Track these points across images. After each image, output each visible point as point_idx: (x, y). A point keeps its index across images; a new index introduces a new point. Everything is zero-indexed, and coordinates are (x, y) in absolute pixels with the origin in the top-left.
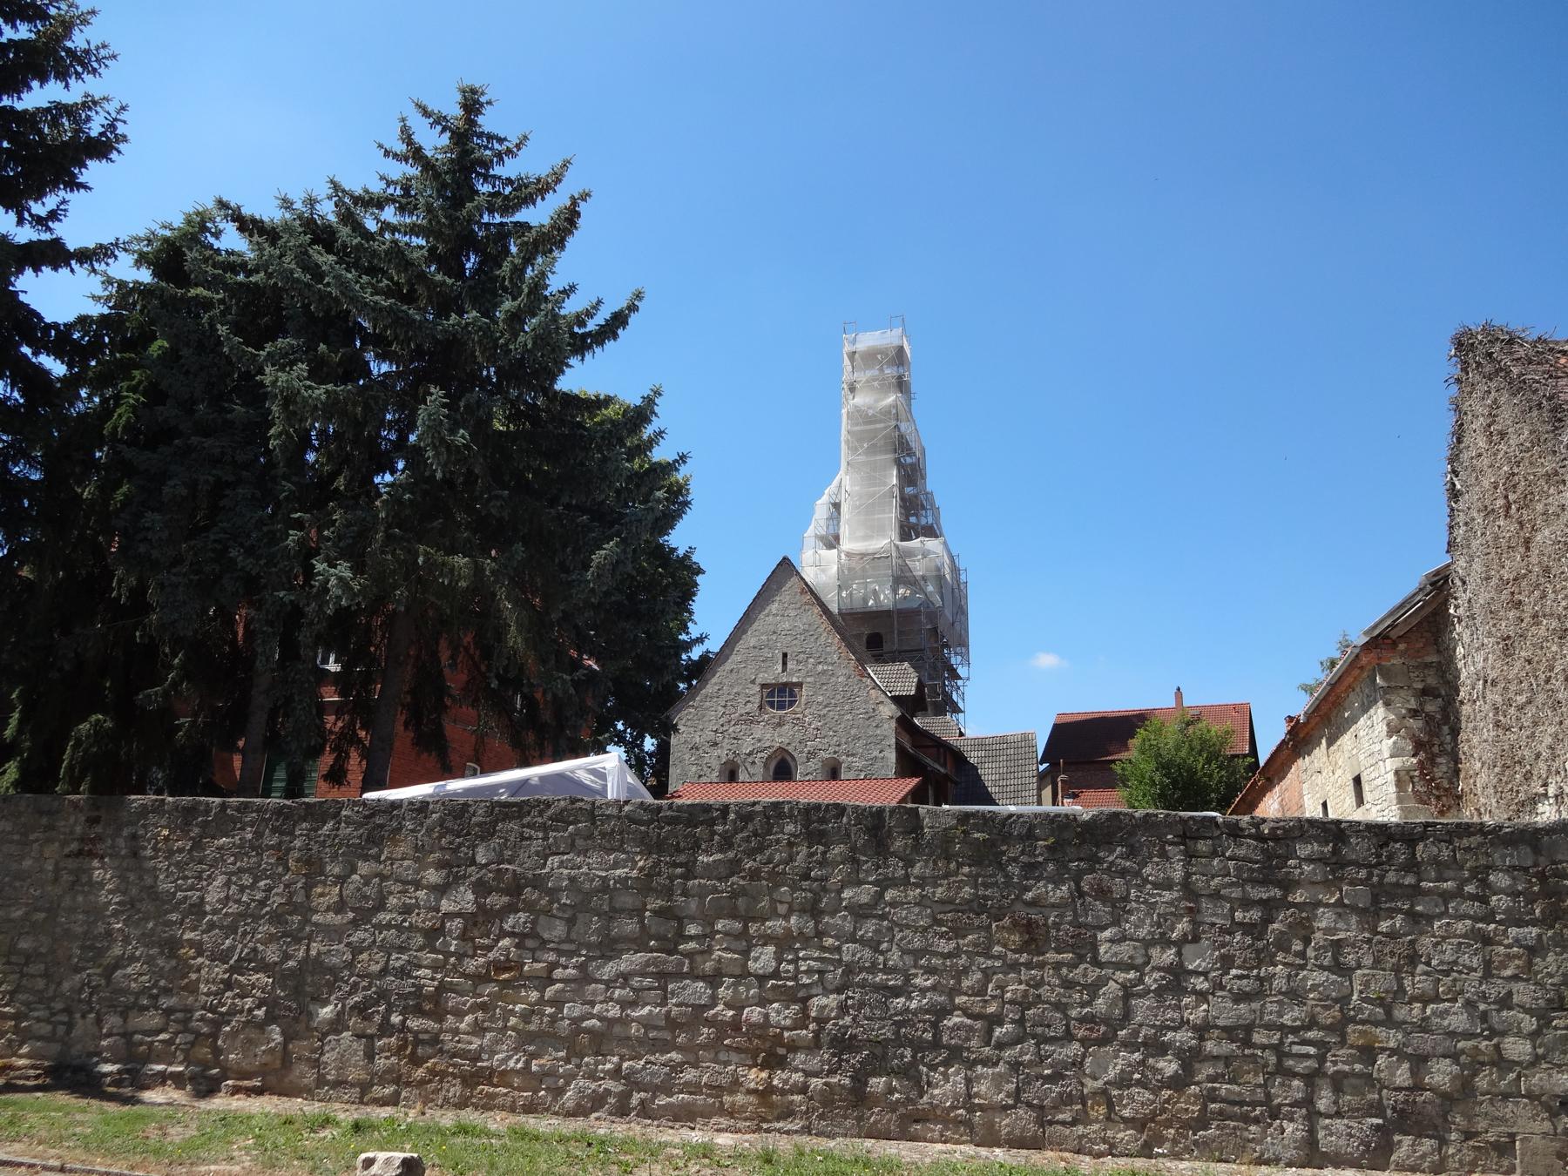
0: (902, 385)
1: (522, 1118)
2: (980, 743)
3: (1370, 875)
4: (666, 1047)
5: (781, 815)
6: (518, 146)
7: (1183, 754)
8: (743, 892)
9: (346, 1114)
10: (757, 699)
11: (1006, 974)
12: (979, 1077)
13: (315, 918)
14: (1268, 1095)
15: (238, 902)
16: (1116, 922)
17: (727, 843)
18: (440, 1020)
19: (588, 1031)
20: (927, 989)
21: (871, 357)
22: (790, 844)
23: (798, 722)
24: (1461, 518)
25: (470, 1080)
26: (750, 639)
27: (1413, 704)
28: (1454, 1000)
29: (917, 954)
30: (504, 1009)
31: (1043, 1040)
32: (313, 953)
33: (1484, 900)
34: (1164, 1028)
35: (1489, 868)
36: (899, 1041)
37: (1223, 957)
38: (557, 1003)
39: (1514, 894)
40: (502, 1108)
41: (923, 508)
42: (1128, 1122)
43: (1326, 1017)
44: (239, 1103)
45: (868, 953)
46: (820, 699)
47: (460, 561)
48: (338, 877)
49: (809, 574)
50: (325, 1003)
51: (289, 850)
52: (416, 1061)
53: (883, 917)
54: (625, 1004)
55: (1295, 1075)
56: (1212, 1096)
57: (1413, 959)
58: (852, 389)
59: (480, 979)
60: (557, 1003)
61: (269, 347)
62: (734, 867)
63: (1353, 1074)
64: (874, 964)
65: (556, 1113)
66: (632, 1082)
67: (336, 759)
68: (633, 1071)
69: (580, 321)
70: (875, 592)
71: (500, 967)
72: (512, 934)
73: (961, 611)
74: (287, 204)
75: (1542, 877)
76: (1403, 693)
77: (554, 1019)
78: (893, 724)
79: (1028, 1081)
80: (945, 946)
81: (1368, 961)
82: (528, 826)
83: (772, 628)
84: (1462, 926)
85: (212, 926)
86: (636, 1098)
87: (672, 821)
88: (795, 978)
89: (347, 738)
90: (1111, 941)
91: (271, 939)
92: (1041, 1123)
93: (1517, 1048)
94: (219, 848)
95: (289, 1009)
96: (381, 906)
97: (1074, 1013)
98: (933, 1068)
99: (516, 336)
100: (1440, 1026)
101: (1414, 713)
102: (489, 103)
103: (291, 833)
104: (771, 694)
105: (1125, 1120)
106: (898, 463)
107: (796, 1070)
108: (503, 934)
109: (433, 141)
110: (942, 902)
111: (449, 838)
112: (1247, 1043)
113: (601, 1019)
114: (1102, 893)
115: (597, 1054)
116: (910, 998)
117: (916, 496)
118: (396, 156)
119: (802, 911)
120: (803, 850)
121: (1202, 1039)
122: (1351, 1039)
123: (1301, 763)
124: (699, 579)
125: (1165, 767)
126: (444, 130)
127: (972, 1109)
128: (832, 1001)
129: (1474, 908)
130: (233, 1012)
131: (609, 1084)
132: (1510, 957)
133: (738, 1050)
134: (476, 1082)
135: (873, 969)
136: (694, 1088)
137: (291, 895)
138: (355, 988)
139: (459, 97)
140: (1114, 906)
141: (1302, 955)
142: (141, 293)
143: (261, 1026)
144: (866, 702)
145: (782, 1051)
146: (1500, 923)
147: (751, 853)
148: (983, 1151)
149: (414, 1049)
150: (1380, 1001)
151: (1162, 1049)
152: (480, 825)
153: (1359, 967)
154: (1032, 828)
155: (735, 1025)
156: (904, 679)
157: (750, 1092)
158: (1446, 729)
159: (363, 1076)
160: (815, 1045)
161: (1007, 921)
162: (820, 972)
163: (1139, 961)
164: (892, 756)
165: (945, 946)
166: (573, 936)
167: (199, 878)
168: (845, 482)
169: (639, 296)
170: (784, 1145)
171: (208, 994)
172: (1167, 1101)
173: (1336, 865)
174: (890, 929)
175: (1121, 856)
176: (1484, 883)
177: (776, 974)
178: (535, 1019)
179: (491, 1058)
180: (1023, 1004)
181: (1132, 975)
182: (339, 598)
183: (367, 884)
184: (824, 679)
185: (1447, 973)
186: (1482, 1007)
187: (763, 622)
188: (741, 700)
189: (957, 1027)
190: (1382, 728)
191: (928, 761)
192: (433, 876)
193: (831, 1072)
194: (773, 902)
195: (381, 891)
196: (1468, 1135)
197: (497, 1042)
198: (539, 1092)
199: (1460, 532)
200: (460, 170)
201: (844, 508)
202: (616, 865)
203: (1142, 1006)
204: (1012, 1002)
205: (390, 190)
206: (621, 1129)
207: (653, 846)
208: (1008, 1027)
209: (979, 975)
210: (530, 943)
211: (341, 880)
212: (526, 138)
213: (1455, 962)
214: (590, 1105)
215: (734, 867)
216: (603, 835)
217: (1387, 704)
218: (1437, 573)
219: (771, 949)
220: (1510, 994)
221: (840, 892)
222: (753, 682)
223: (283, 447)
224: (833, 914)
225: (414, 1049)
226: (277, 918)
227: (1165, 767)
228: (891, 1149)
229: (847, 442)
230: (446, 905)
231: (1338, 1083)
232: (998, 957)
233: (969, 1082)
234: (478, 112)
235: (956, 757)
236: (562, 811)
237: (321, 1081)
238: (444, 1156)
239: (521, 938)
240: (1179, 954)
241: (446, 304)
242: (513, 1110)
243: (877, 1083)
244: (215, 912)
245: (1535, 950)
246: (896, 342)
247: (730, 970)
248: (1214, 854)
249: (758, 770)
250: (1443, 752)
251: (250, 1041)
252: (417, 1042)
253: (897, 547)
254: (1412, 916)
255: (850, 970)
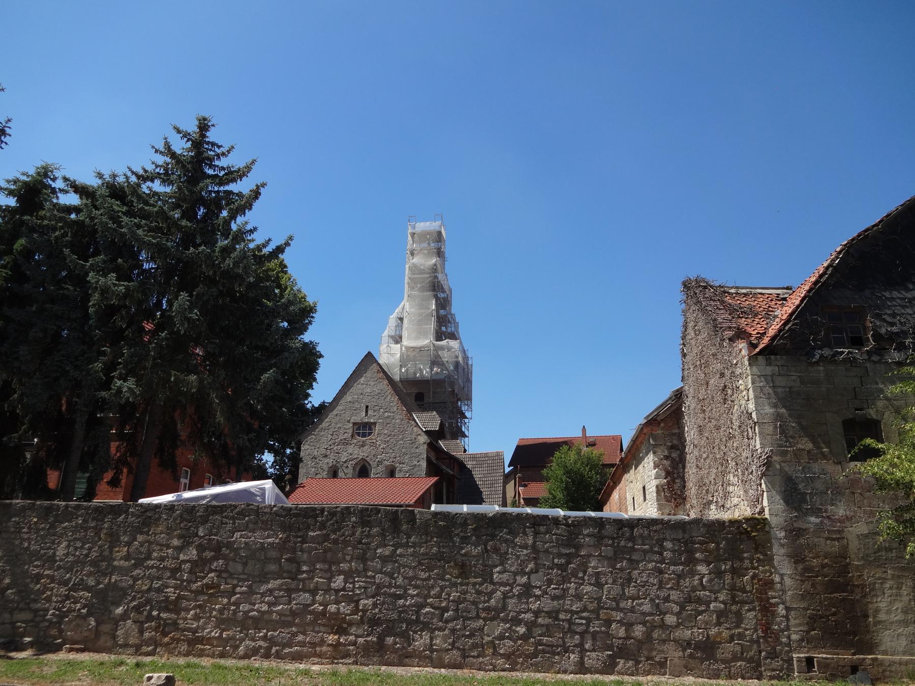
0: (440, 253)
1: (218, 660)
2: (474, 457)
3: (614, 543)
4: (290, 624)
5: (350, 513)
6: (229, 152)
7: (578, 466)
8: (330, 549)
9: (131, 660)
10: (350, 431)
11: (451, 588)
12: (436, 637)
13: (116, 563)
14: (564, 642)
15: (74, 555)
16: (502, 564)
17: (323, 526)
18: (178, 613)
19: (252, 617)
20: (414, 596)
21: (422, 237)
22: (353, 527)
23: (373, 444)
24: (686, 367)
25: (192, 643)
26: (348, 397)
27: (666, 453)
28: (646, 598)
29: (411, 579)
30: (210, 607)
31: (465, 619)
32: (113, 580)
33: (661, 554)
34: (520, 612)
35: (665, 539)
36: (401, 620)
37: (548, 579)
38: (237, 604)
39: (673, 551)
40: (208, 656)
41: (449, 322)
42: (502, 656)
43: (591, 607)
44: (72, 656)
45: (387, 579)
46: (386, 432)
47: (193, 377)
48: (127, 543)
49: (383, 359)
50: (118, 606)
51: (101, 529)
52: (165, 634)
53: (396, 562)
54: (270, 604)
55: (576, 633)
56: (540, 643)
57: (629, 580)
58: (412, 254)
59: (198, 592)
60: (237, 604)
61: (91, 261)
62: (326, 538)
63: (601, 632)
64: (390, 584)
65: (235, 658)
66: (272, 642)
67: (115, 474)
68: (273, 637)
69: (259, 248)
70: (420, 369)
71: (208, 586)
72: (215, 571)
73: (469, 381)
74: (100, 176)
75: (686, 543)
76: (662, 448)
77: (235, 613)
78: (426, 446)
79: (458, 638)
80: (423, 575)
81: (610, 581)
82: (226, 517)
83: (360, 391)
84: (650, 566)
85: (59, 567)
86: (274, 650)
87: (296, 515)
88: (353, 591)
89: (122, 461)
90: (499, 572)
91: (90, 574)
92: (464, 657)
93: (670, 619)
94: (64, 528)
95: (99, 609)
96: (149, 557)
97: (481, 606)
98: (415, 632)
99: (224, 260)
100: (639, 610)
101: (666, 458)
102: (213, 125)
103: (103, 520)
104: (359, 429)
105: (501, 655)
106: (436, 297)
107: (352, 634)
108: (211, 571)
109: (180, 146)
110: (423, 554)
111: (185, 523)
112: (557, 619)
113: (258, 611)
114: (496, 550)
115: (255, 628)
116: (406, 600)
117: (446, 316)
118: (161, 152)
119: (358, 559)
120: (360, 530)
121: (537, 617)
122: (601, 616)
123: (626, 476)
124: (320, 361)
125: (568, 472)
126: (188, 141)
127: (432, 651)
128: (370, 602)
129: (657, 557)
130: (70, 610)
131: (261, 643)
132: (670, 579)
133: (324, 625)
134: (195, 644)
135: (390, 586)
136: (302, 644)
137: (102, 551)
138: (134, 598)
139: (197, 123)
140: (501, 556)
141: (582, 578)
142: (9, 212)
143: (85, 617)
144: (411, 434)
145: (345, 626)
146: (667, 564)
147: (334, 532)
148: (436, 670)
149: (164, 628)
150: (614, 599)
151: (518, 622)
152: (201, 516)
153: (607, 584)
154: (466, 520)
155: (324, 613)
156: (431, 421)
157: (329, 645)
158: (680, 465)
159: (137, 642)
160: (362, 622)
161: (452, 564)
162: (365, 588)
163: (511, 581)
164: (424, 464)
165: (423, 575)
166: (246, 571)
167: (53, 543)
168: (406, 306)
169: (291, 238)
170: (342, 669)
171: (56, 602)
172: (520, 646)
173: (599, 539)
174: (399, 567)
175: (505, 533)
176: (661, 546)
177: (344, 589)
178: (226, 612)
179: (203, 631)
180: (458, 602)
181: (507, 588)
182: (128, 398)
183: (142, 546)
184: (388, 421)
185: (643, 586)
186: (657, 601)
187: (356, 388)
188: (342, 431)
189: (428, 613)
190: (652, 464)
191: (444, 467)
192: (176, 542)
193: (368, 635)
194: (344, 555)
195: (149, 550)
196: (648, 659)
197: (206, 623)
198: (227, 648)
199: (686, 372)
200: (195, 164)
201: (405, 321)
202: (268, 537)
203: (511, 602)
204: (453, 601)
205: (158, 170)
206: (266, 664)
207: (285, 528)
208: (451, 613)
209: (438, 589)
210: (224, 575)
211: (129, 544)
212: (233, 147)
213: (647, 581)
214: (251, 653)
215: (326, 538)
216: (263, 522)
217: (654, 453)
218: (678, 390)
219: (342, 577)
220: (669, 595)
221: (376, 550)
222: (349, 421)
223: (96, 312)
224: (372, 561)
225: (164, 628)
226: (94, 563)
227: (568, 472)
228: (394, 670)
229: (408, 283)
230: (182, 557)
231: (594, 636)
232: (447, 580)
233: (432, 639)
234: (207, 130)
235: (461, 465)
236: (243, 509)
237: (116, 645)
238: (183, 676)
239: (219, 573)
240: (529, 578)
241: (188, 240)
242: (213, 656)
243: (390, 640)
244: (61, 560)
245: (680, 577)
246: (437, 229)
247: (321, 587)
248: (547, 532)
249: (350, 471)
250: (679, 477)
251: (78, 625)
252: (166, 625)
253: (434, 345)
254: (630, 561)
255: (379, 587)
